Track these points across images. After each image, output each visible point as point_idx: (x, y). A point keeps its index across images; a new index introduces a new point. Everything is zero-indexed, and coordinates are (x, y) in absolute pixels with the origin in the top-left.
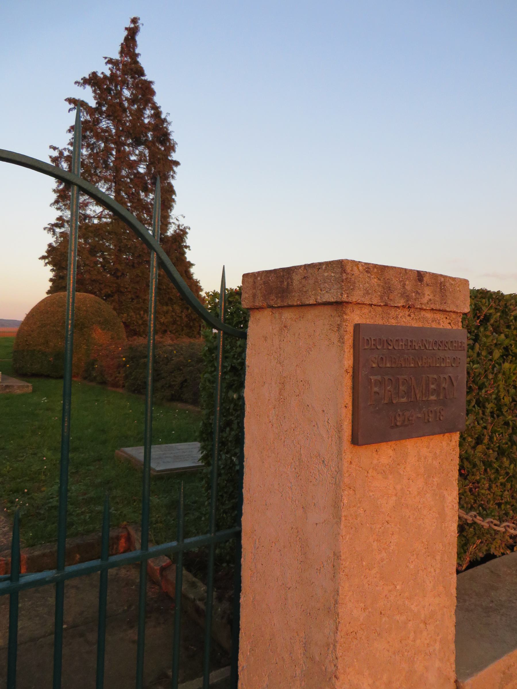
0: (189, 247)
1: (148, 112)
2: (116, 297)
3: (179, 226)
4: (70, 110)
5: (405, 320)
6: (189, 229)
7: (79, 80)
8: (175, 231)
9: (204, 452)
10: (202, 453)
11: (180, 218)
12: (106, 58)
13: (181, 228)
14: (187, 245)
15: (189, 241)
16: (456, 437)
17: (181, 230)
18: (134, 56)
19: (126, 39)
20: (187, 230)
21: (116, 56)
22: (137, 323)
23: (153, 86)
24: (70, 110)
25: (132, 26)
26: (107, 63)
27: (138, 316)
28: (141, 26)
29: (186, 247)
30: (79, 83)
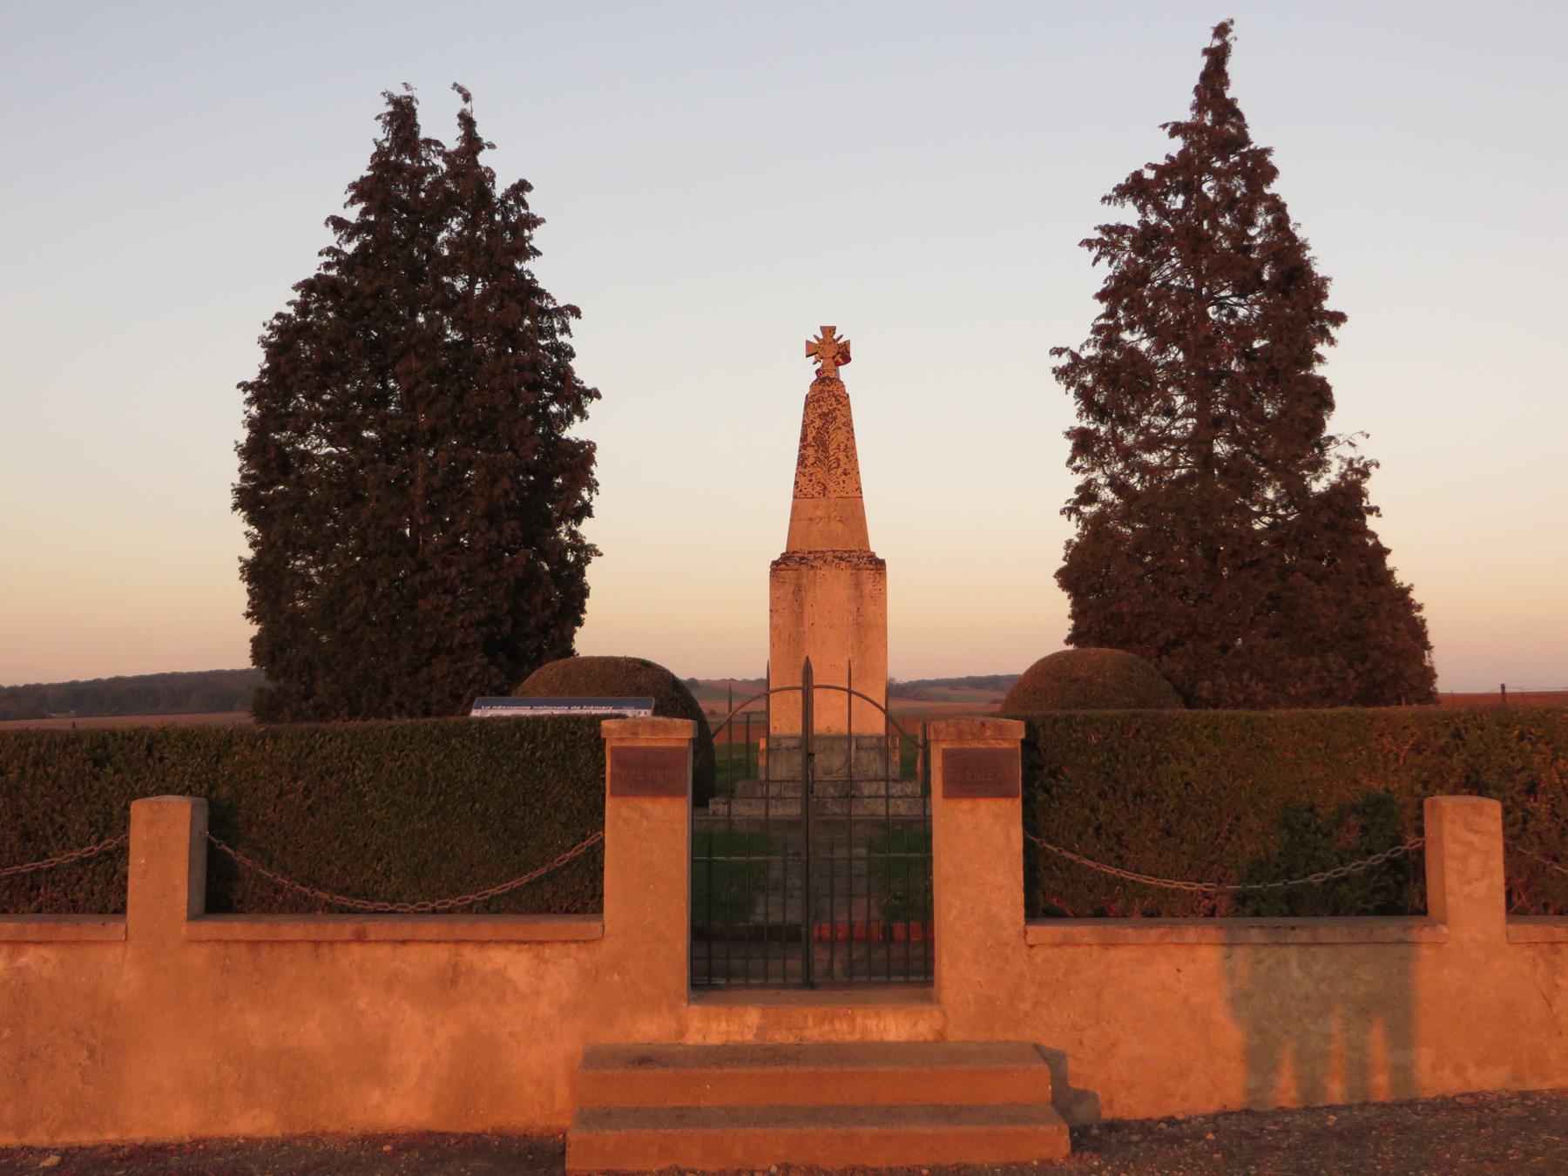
0: (1377, 509)
1: (1263, 220)
2: (1189, 646)
3: (1350, 463)
4: (1097, 259)
5: (975, 745)
6: (1378, 465)
7: (1109, 192)
8: (1343, 476)
9: (333, 272)
10: (328, 266)
11: (1359, 440)
12: (1165, 126)
13: (1356, 465)
14: (1372, 504)
15: (1375, 490)
16: (590, 641)
17: (1357, 471)
18: (1228, 111)
19: (1205, 77)
20: (1373, 470)
21: (1187, 116)
22: (1233, 698)
23: (1270, 159)
24: (1097, 259)
25: (1217, 43)
26: (1172, 134)
27: (1236, 684)
28: (1232, 42)
29: (1371, 510)
30: (1109, 198)
